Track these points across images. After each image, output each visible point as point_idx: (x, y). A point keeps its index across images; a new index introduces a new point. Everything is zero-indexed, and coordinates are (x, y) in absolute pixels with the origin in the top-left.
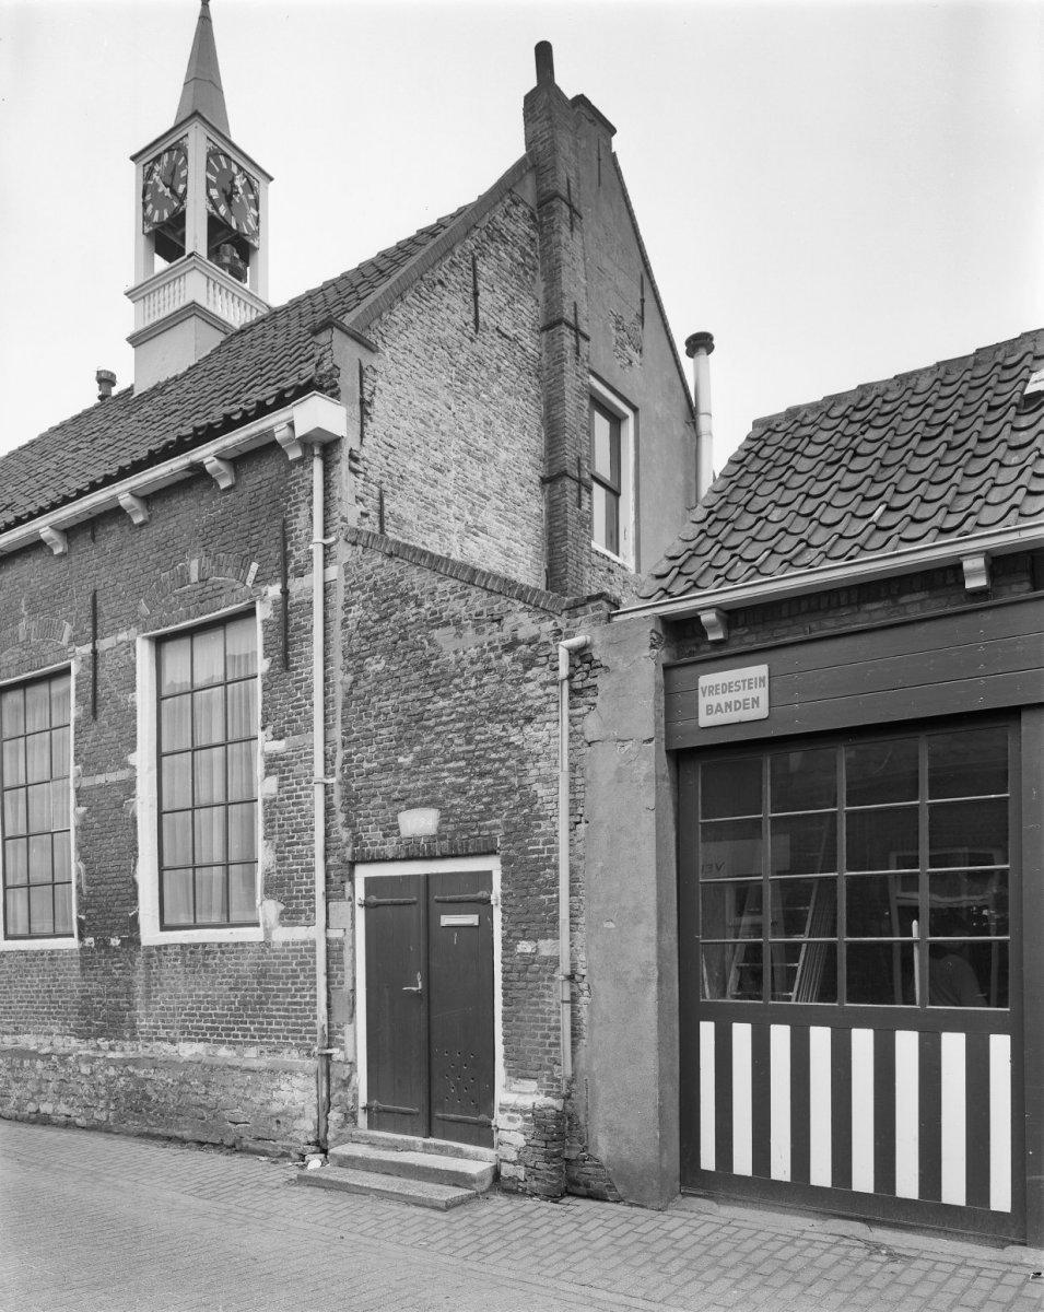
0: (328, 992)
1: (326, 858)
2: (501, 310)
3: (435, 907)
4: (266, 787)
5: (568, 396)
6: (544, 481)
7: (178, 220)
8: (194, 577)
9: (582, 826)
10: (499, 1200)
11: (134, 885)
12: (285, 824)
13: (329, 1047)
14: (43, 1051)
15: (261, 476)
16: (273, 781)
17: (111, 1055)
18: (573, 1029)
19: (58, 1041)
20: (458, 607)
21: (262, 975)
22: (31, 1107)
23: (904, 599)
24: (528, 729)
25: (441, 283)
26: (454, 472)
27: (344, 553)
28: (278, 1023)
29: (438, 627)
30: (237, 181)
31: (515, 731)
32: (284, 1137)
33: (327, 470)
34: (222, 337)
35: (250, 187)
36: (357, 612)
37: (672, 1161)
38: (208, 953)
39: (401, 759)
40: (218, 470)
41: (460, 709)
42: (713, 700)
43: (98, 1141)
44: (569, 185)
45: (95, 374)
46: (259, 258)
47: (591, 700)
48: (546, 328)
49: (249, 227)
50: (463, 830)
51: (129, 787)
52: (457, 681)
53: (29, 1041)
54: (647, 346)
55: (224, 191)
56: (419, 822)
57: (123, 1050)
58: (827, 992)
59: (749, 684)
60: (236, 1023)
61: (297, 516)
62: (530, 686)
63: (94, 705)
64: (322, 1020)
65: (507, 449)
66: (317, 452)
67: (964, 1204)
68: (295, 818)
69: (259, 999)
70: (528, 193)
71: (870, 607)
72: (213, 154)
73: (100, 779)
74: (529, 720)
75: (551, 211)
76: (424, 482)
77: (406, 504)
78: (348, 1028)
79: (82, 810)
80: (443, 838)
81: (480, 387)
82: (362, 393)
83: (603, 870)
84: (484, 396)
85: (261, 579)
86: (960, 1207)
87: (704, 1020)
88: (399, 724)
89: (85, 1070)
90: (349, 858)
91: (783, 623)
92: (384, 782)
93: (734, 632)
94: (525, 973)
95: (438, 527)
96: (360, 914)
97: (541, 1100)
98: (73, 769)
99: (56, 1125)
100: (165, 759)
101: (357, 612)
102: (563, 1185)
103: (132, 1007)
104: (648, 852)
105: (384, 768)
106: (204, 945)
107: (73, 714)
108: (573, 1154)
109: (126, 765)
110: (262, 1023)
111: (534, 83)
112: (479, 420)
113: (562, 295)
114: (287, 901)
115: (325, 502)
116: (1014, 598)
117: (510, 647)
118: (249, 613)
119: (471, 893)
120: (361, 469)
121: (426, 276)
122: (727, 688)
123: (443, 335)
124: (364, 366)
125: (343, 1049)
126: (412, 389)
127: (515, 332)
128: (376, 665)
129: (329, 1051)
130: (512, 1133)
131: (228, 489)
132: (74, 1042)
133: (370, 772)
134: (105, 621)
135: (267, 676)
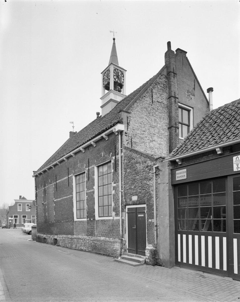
0: (122, 228)
1: (122, 204)
2: (158, 97)
3: (138, 213)
4: (113, 192)
5: (173, 111)
6: (169, 128)
7: (109, 84)
8: (103, 156)
9: (158, 199)
10: (145, 265)
11: (94, 209)
12: (116, 200)
13: (122, 238)
14: (82, 238)
15: (112, 137)
16: (114, 191)
17: (91, 239)
18: (157, 235)
19: (84, 236)
20: (140, 160)
21: (113, 225)
22: (80, 248)
23: (209, 156)
24: (150, 181)
25: (145, 96)
26: (147, 131)
27: (124, 151)
28: (115, 234)
29: (137, 164)
30: (120, 74)
31: (148, 182)
32: (116, 254)
33: (121, 136)
34: (116, 104)
35: (122, 73)
36: (126, 161)
37: (174, 260)
38: (105, 221)
39: (132, 187)
40: (105, 137)
41: (140, 178)
42: (180, 175)
43: (89, 254)
44: (173, 69)
45: (96, 113)
46: (124, 87)
47: (159, 176)
48: (169, 98)
49: (122, 81)
50: (141, 200)
51: (94, 192)
52: (140, 173)
53: (80, 236)
54: (196, 94)
55: (117, 76)
56: (135, 198)
57: (93, 238)
58: (210, 229)
59: (184, 172)
60: (109, 234)
61: (117, 144)
62: (150, 174)
63: (89, 178)
64: (121, 233)
65: (160, 124)
66: (120, 133)
67: (219, 269)
68: (117, 197)
69: (112, 229)
70: (165, 73)
71: (204, 157)
72: (115, 70)
73: (89, 191)
74: (150, 180)
75: (169, 75)
76: (141, 134)
77: (137, 139)
78: (125, 235)
79: (87, 196)
80: (138, 201)
81: (153, 114)
82: (127, 121)
83: (161, 207)
84: (154, 115)
85: (112, 156)
86: (236, 274)
87: (234, 238)
88: (132, 181)
89: (88, 242)
90: (125, 205)
91: (191, 161)
92: (130, 191)
93: (183, 162)
94: (151, 224)
95: (144, 142)
96: (127, 214)
97: (152, 248)
98: (86, 189)
99: (84, 251)
100: (99, 187)
101: (126, 161)
102: (155, 263)
103: (94, 231)
104: (168, 203)
105: (130, 189)
106: (104, 220)
107: (86, 180)
108: (157, 258)
109: (93, 189)
110: (112, 234)
111: (167, 50)
112: (153, 120)
113: (172, 91)
114: (116, 212)
115: (121, 142)
116: (227, 155)
117: (147, 167)
118: (110, 162)
119: (141, 211)
120: (127, 135)
121: (141, 96)
122: (180, 173)
123: (145, 106)
124: (128, 116)
125: (124, 238)
126: (138, 118)
127: (162, 101)
128: (128, 171)
129: (122, 239)
130: (148, 253)
131: (107, 140)
132: (86, 237)
133: (128, 189)
134: (90, 164)
135: (113, 173)
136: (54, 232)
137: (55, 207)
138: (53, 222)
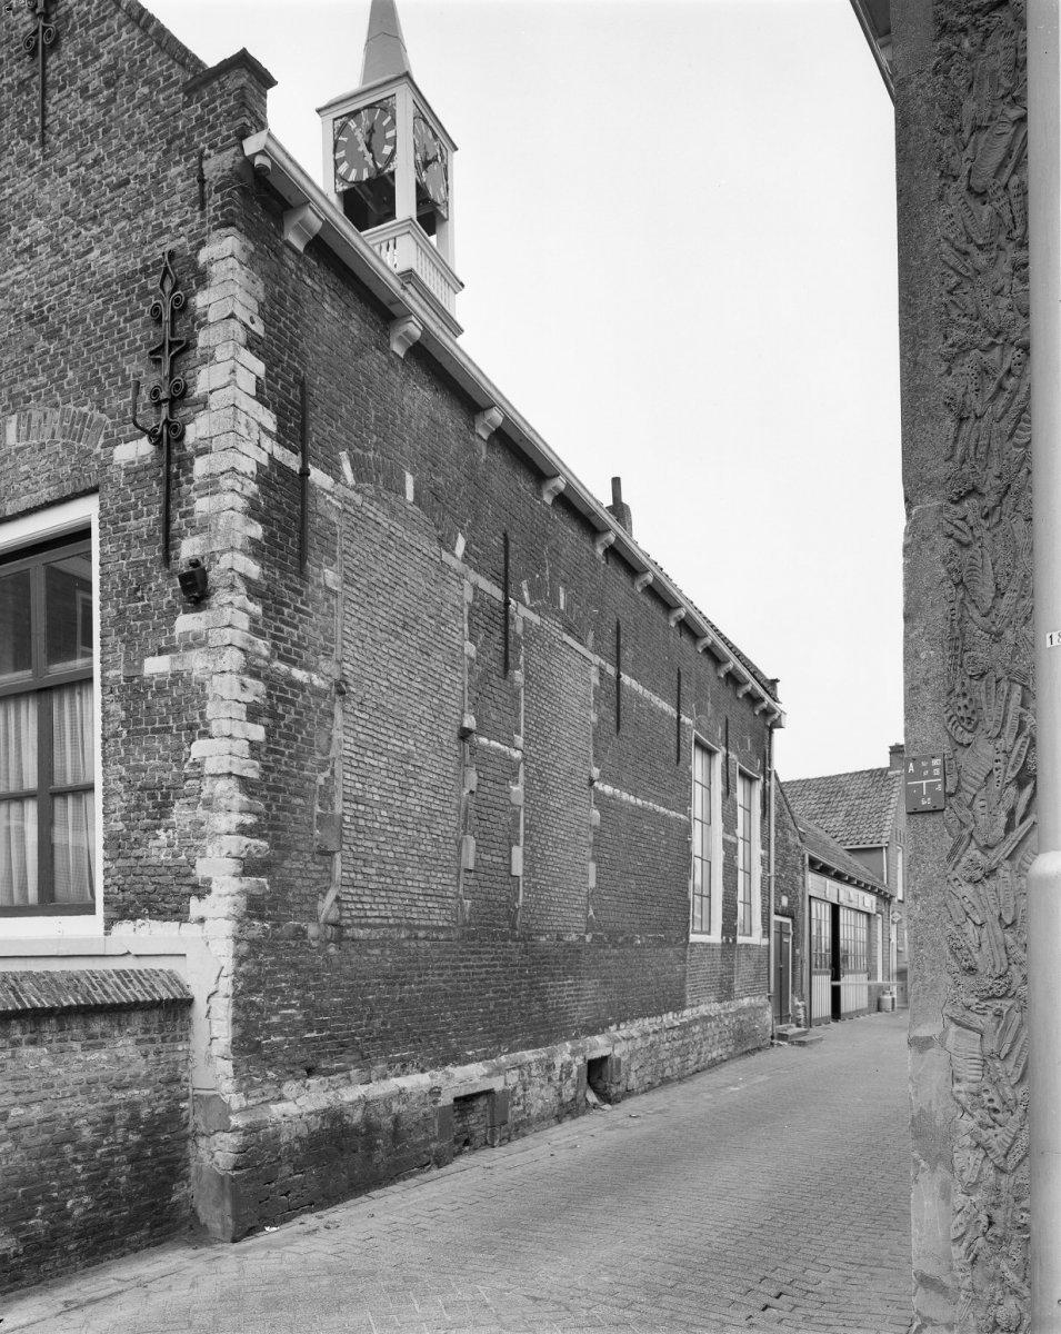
136: (580, 1014)
137: (598, 832)
138: (574, 937)
